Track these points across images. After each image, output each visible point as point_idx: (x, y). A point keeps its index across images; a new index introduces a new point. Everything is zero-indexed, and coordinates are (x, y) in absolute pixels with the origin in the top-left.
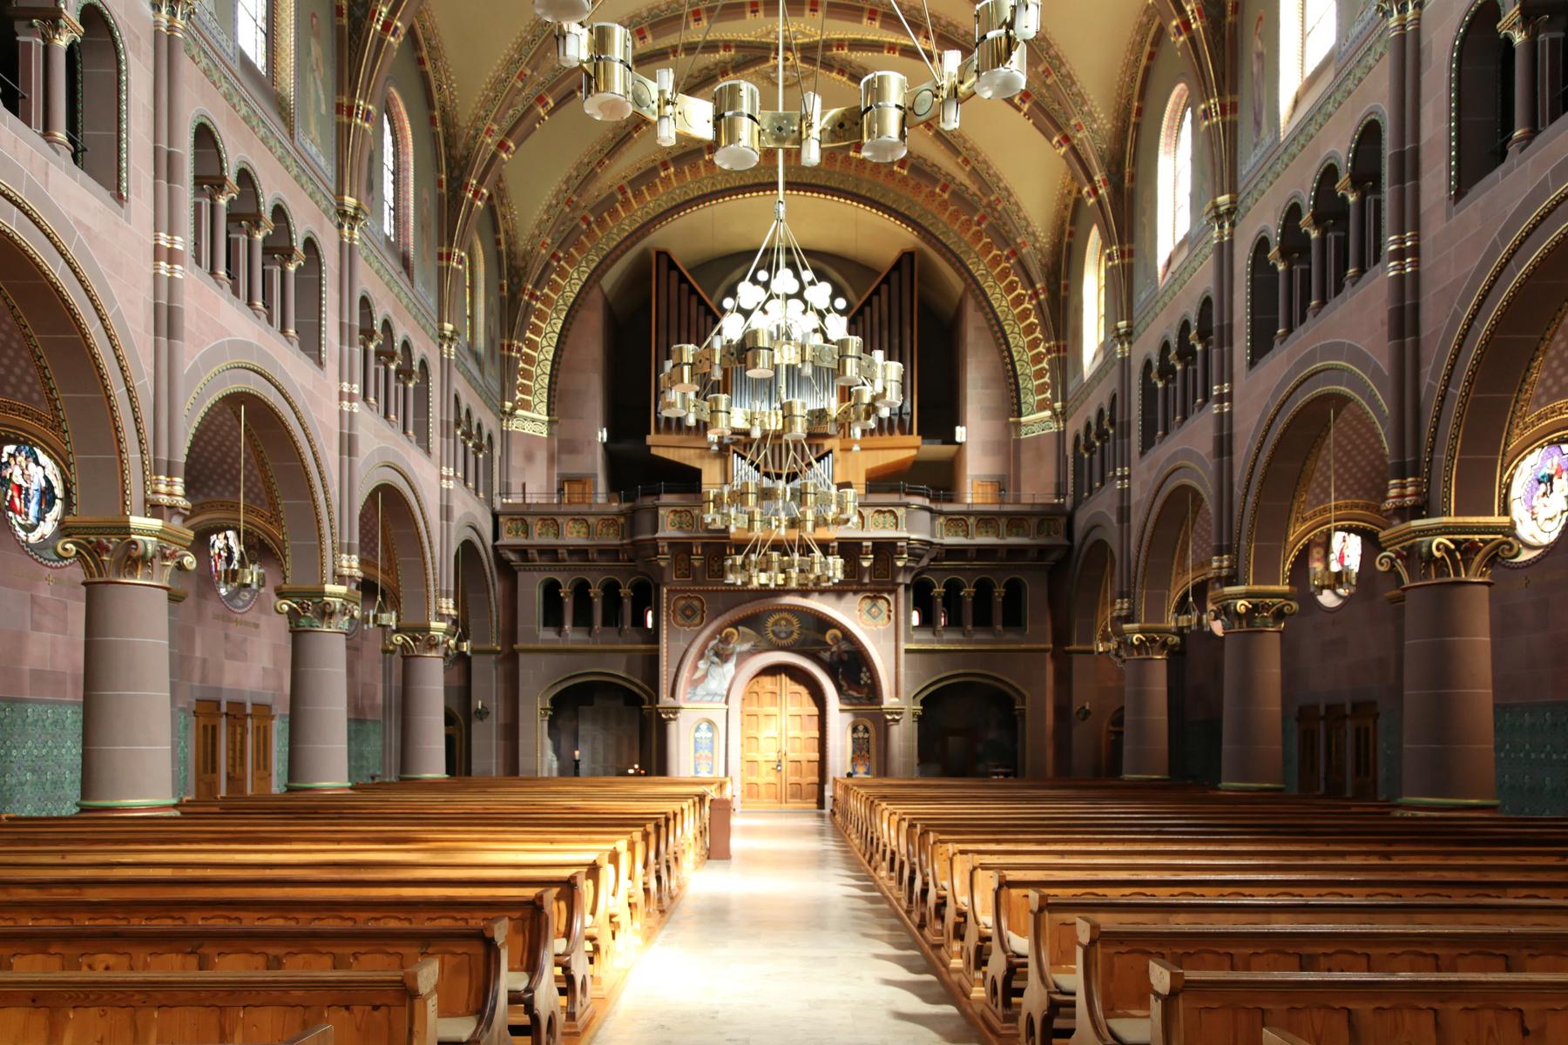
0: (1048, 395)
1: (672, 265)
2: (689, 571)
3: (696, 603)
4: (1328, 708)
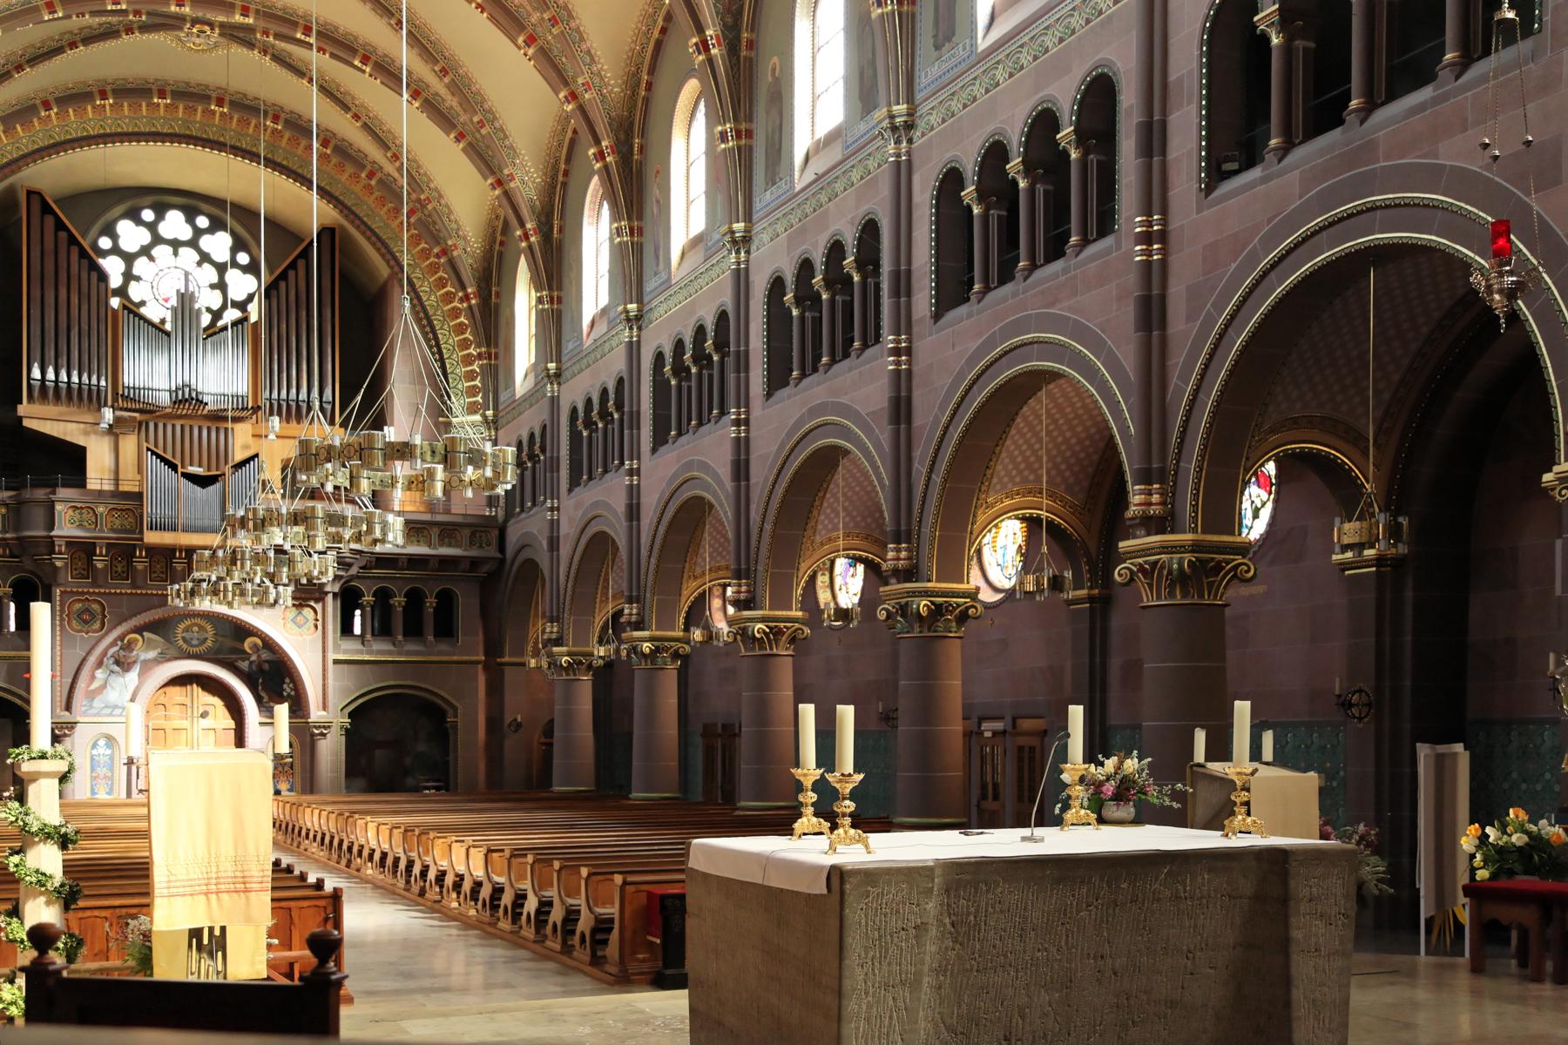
0: (479, 398)
1: (46, 209)
2: (87, 570)
3: (96, 607)
4: (724, 726)
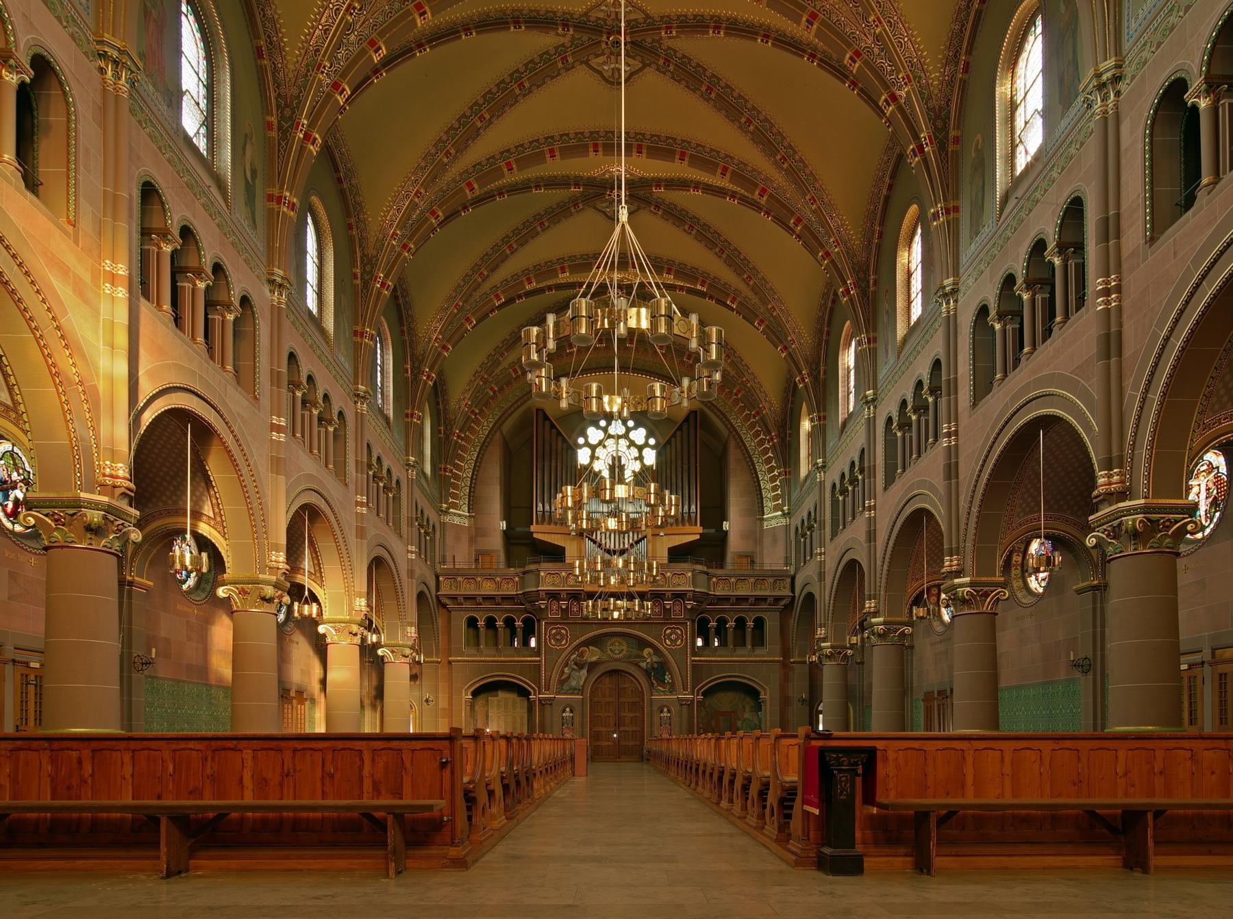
1: (546, 418)
4: (939, 692)
